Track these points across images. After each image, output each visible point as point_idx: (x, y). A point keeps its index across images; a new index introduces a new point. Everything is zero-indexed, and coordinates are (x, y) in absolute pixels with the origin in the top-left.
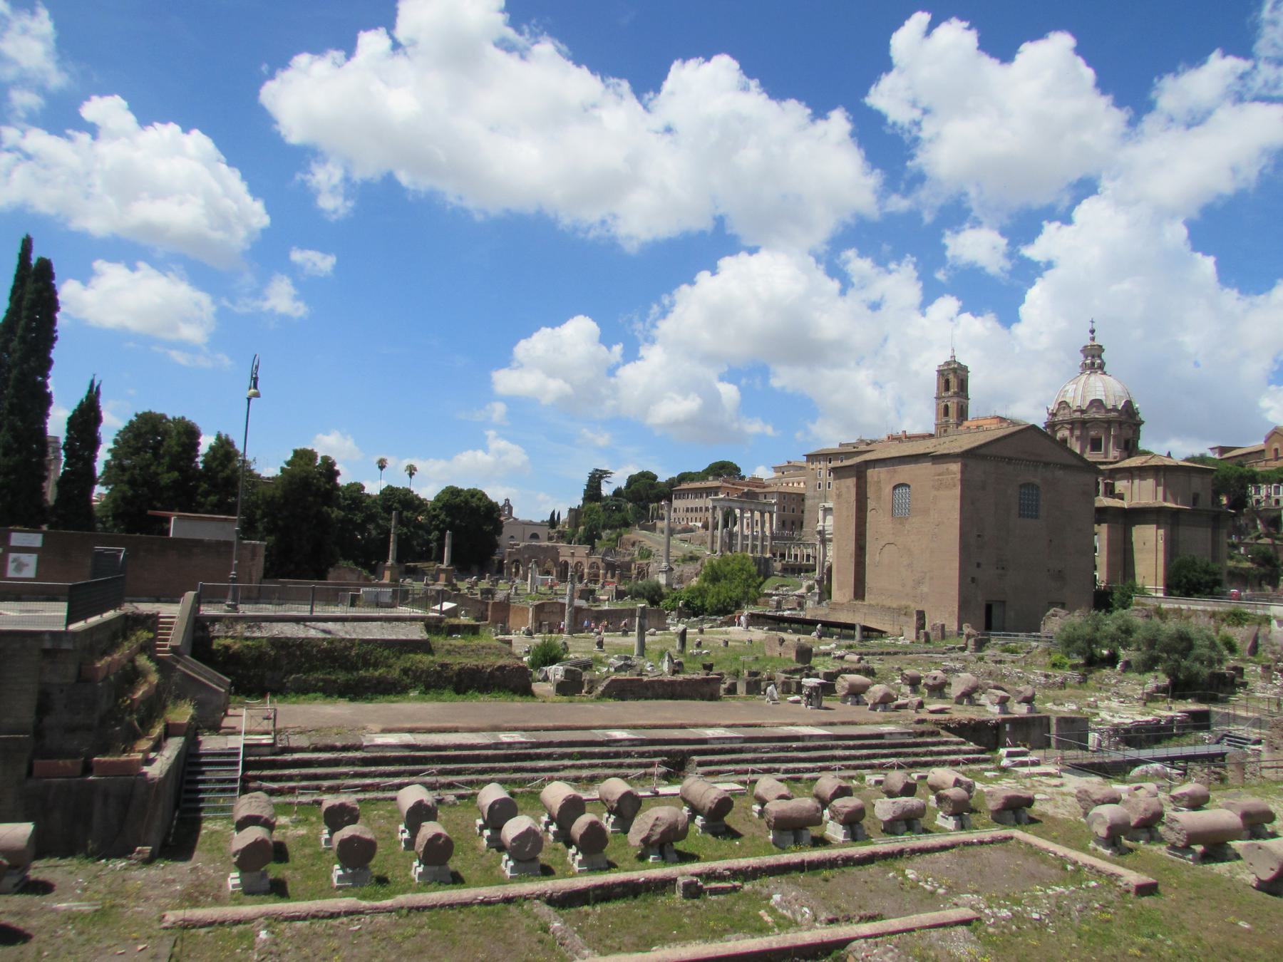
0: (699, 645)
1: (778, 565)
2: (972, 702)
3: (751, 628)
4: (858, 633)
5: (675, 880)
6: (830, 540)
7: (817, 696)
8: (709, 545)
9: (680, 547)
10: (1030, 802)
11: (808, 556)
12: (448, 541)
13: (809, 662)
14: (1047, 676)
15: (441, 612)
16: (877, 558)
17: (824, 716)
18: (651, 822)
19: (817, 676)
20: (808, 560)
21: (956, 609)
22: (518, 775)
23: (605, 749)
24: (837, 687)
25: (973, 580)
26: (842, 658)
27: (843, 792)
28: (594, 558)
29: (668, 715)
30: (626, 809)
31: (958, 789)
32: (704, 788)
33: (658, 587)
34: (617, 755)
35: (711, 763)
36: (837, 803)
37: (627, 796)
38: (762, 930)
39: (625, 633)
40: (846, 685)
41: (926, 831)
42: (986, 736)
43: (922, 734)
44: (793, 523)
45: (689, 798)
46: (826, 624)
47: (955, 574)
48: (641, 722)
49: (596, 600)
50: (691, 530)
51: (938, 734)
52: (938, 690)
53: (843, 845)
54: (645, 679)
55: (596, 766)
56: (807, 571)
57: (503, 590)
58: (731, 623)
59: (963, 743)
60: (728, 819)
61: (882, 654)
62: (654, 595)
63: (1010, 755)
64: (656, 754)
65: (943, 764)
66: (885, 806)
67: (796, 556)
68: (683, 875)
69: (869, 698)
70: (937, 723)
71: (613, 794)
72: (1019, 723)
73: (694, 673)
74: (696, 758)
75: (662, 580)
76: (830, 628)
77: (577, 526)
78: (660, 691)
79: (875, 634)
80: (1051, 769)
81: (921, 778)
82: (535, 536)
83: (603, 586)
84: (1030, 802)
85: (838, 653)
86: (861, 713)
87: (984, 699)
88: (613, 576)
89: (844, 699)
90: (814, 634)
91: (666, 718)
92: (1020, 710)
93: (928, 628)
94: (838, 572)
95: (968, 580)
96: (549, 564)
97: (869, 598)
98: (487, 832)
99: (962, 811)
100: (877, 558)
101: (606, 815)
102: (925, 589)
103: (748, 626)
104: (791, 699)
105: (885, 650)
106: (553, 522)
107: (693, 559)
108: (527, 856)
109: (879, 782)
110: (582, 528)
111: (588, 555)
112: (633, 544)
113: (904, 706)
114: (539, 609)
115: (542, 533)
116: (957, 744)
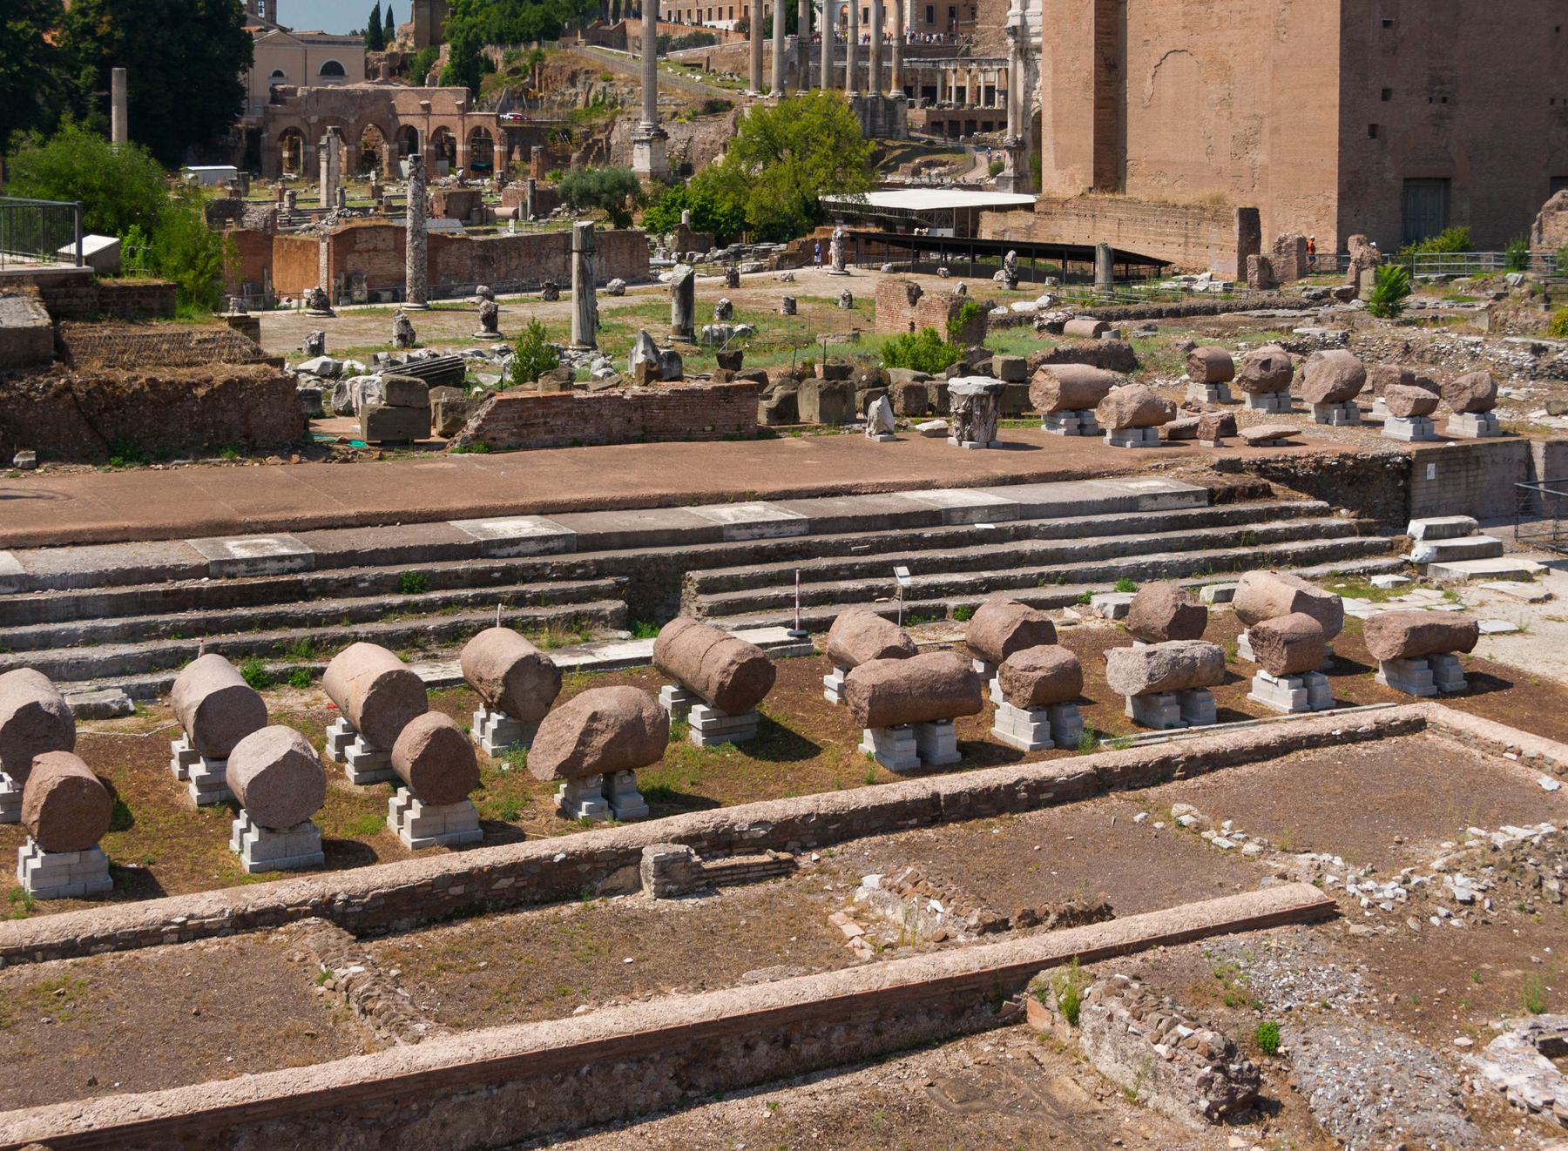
0: (727, 312)
1: (917, 115)
2: (1353, 418)
3: (850, 268)
4: (1100, 269)
5: (638, 853)
6: (1039, 49)
7: (984, 418)
8: (751, 74)
9: (682, 82)
10: (1469, 636)
11: (990, 90)
12: (118, 89)
13: (980, 342)
14: (1537, 350)
15: (79, 258)
16: (1148, 87)
17: (1005, 463)
18: (579, 725)
19: (987, 371)
20: (990, 99)
21: (1334, 204)
22: (274, 635)
23: (480, 564)
24: (1034, 396)
25: (1373, 130)
26: (1057, 328)
27: (1032, 634)
28: (477, 118)
29: (632, 477)
30: (527, 696)
31: (1301, 617)
32: (705, 642)
33: (628, 185)
34: (509, 576)
35: (734, 584)
36: (1019, 659)
37: (524, 666)
38: (840, 957)
39: (553, 295)
40: (1054, 387)
41: (1227, 716)
42: (1378, 494)
43: (1229, 495)
44: (952, 12)
45: (673, 666)
46: (1027, 250)
47: (1331, 118)
48: (566, 497)
49: (488, 218)
50: (709, 40)
51: (1268, 493)
52: (1274, 387)
53: (1037, 753)
54: (579, 394)
55: (463, 603)
56: (988, 127)
57: (262, 200)
58: (803, 258)
59: (1464, 531)
60: (770, 706)
61: (1158, 314)
62: (616, 197)
63: (1430, 534)
64: (601, 570)
65: (1279, 561)
66: (1130, 663)
67: (961, 90)
68: (656, 841)
69: (1104, 416)
70: (1262, 468)
71: (492, 664)
72: (1459, 458)
73: (702, 375)
74: (697, 575)
75: (641, 162)
76: (1040, 259)
77: (435, 42)
78: (617, 424)
79: (1144, 269)
80: (1529, 563)
81: (1226, 596)
82: (333, 70)
83: (503, 184)
84: (1469, 636)
85: (1050, 316)
86: (1085, 452)
87: (1379, 408)
88: (526, 158)
89: (1052, 419)
90: (1000, 275)
91: (627, 485)
92: (1463, 427)
93: (1266, 248)
94: (1056, 125)
95: (1361, 133)
96: (371, 134)
97: (1137, 186)
98: (198, 769)
99: (1322, 661)
100: (1148, 87)
101: (481, 714)
102: (1260, 156)
103: (843, 263)
104: (924, 427)
105: (1165, 306)
106: (377, 35)
107: (714, 108)
108: (294, 816)
109: (1122, 611)
110: (446, 48)
111: (466, 109)
112: (572, 80)
113: (1189, 433)
114: (343, 243)
115: (352, 60)
116: (1311, 513)
